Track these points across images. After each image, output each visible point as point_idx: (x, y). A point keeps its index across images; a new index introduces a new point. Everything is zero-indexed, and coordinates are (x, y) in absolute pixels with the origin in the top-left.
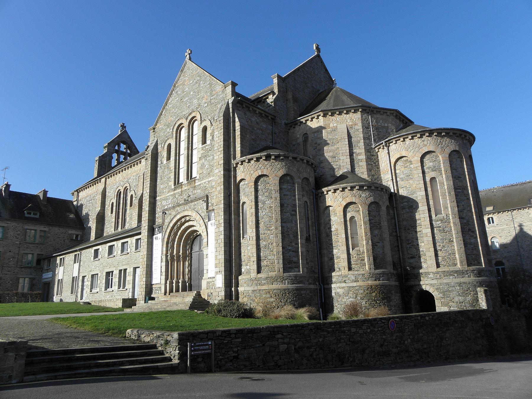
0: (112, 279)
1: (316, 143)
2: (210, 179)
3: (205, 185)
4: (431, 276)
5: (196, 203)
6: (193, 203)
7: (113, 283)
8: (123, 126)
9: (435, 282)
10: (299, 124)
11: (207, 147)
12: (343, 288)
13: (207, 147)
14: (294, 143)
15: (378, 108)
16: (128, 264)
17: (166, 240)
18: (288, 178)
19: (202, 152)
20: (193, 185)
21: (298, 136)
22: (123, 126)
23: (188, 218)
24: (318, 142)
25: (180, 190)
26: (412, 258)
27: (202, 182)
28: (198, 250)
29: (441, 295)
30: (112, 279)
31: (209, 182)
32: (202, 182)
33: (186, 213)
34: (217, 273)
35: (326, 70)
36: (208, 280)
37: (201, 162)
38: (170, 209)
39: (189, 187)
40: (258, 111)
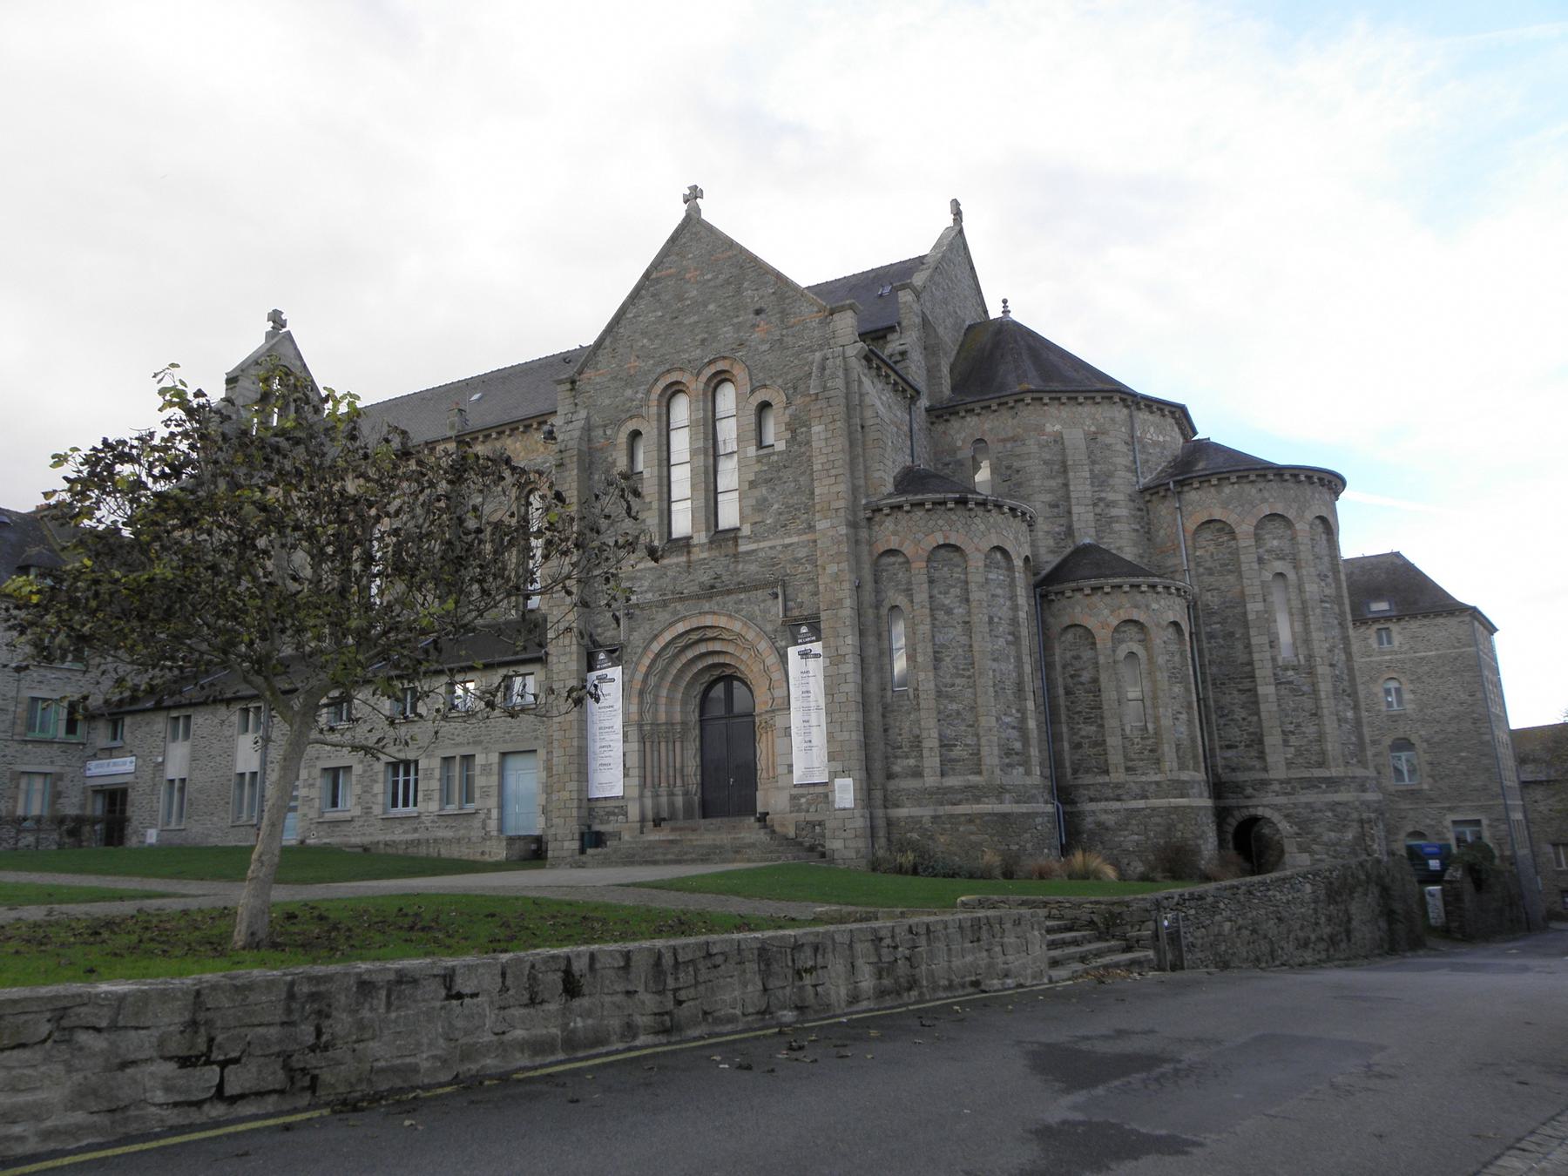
0: (416, 781)
1: (1008, 468)
2: (787, 541)
3: (773, 553)
4: (1276, 787)
5: (742, 596)
6: (734, 597)
7: (420, 795)
8: (277, 319)
9: (1282, 800)
10: (962, 414)
11: (775, 458)
12: (1117, 811)
13: (775, 458)
14: (948, 459)
15: (1134, 395)
16: (477, 743)
17: (637, 686)
18: (999, 555)
19: (757, 468)
20: (731, 551)
21: (959, 443)
22: (277, 319)
23: (710, 634)
24: (1016, 465)
25: (684, 559)
26: (1229, 747)
27: (762, 545)
28: (723, 712)
29: (1295, 828)
30: (416, 781)
31: (786, 546)
32: (762, 545)
33: (708, 621)
34: (834, 775)
35: (972, 268)
36: (795, 791)
37: (757, 493)
38: (650, 604)
39: (715, 553)
40: (893, 377)
